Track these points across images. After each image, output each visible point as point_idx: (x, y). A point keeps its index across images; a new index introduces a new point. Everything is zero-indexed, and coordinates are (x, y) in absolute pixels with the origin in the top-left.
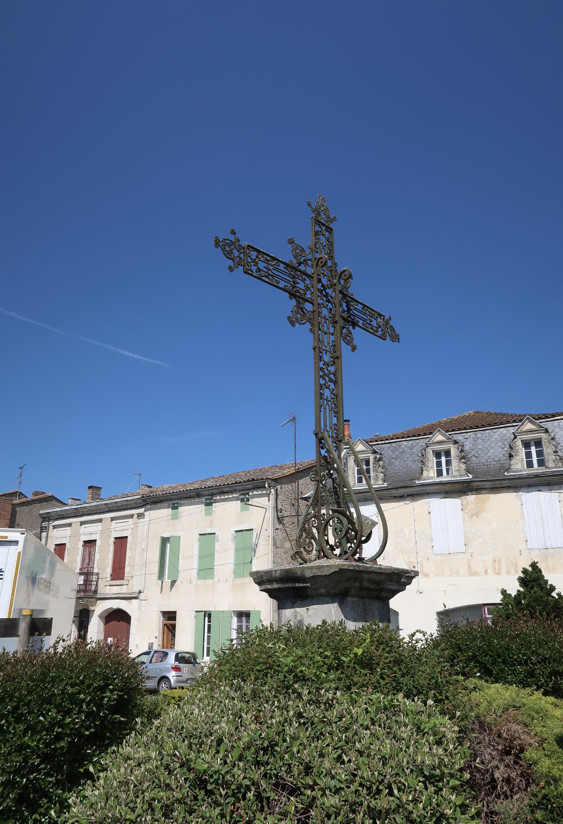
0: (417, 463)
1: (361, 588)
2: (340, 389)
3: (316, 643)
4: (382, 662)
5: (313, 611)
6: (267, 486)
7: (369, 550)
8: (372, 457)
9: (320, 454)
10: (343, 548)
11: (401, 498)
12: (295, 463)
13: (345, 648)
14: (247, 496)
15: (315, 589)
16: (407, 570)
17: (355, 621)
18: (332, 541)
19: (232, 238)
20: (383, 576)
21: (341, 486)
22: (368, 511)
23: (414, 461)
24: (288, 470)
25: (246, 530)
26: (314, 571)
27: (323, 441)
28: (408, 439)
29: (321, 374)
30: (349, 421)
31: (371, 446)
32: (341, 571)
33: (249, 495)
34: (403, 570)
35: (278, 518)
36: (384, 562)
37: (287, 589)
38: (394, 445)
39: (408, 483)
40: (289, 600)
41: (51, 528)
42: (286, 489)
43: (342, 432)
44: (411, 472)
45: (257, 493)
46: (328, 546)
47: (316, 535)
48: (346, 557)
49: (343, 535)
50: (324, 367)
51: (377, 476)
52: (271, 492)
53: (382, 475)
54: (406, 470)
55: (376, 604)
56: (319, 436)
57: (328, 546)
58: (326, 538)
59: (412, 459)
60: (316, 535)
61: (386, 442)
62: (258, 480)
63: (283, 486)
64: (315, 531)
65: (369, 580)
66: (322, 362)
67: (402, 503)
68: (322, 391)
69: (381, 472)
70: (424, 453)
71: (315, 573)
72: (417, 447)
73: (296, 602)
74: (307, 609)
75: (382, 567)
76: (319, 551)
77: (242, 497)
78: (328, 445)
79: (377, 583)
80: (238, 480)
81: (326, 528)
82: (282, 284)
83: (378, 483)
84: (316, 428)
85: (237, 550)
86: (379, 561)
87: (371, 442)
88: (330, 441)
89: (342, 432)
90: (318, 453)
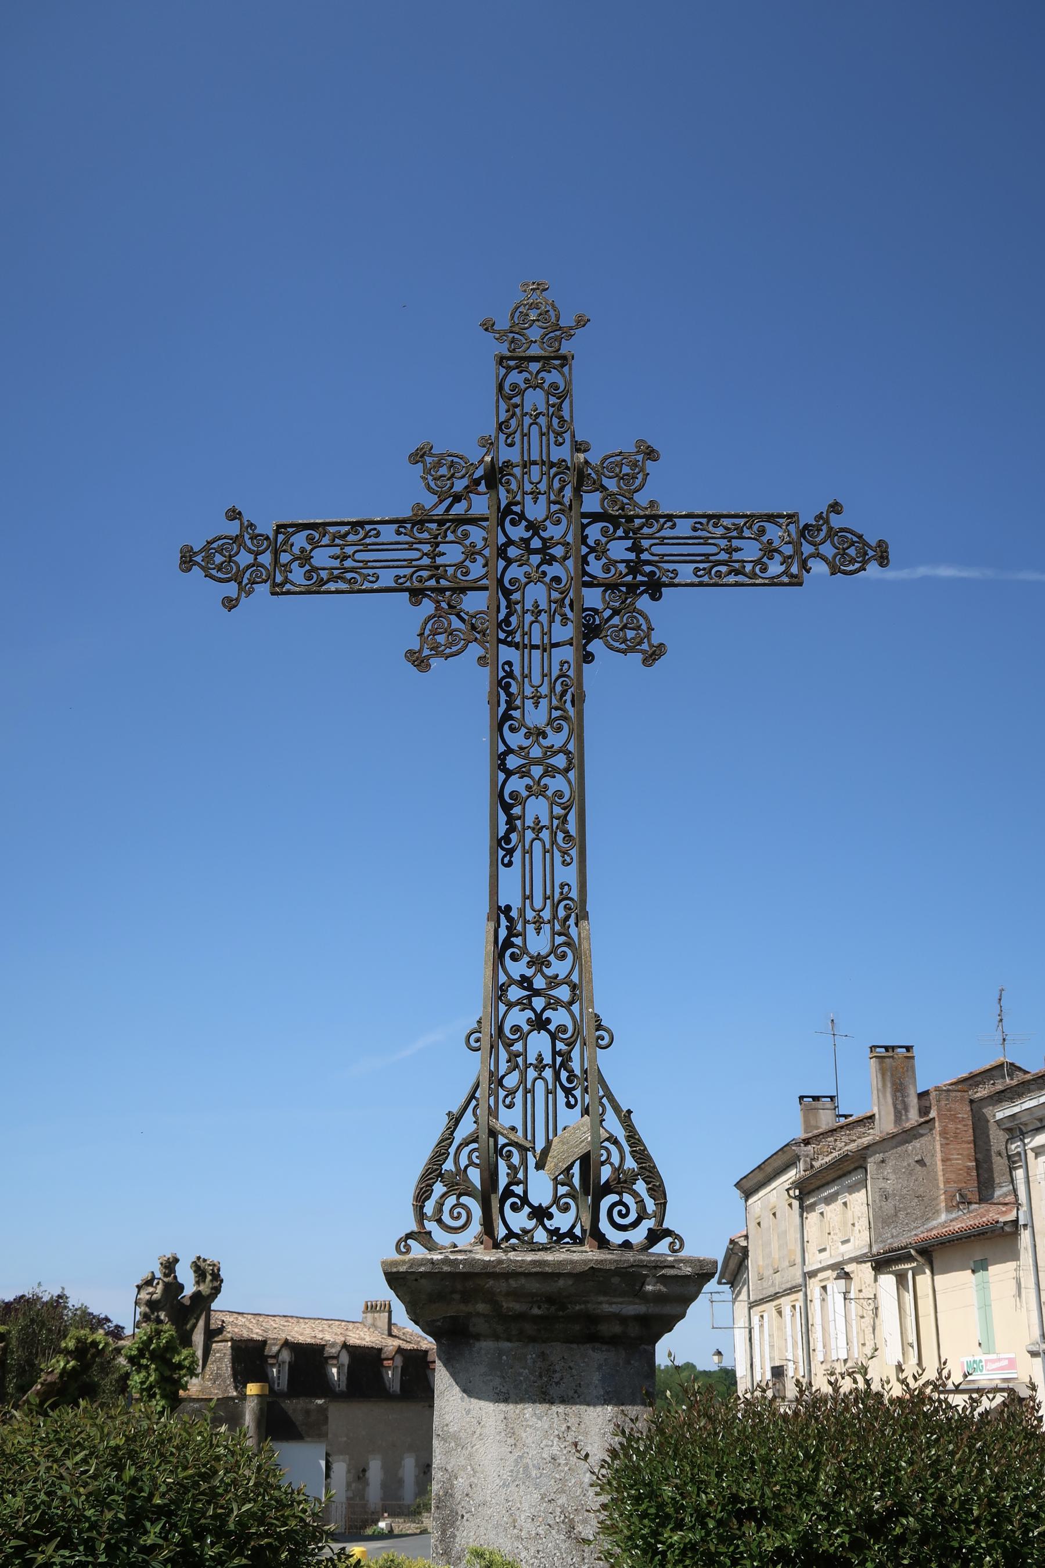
17: (506, 1401)
19: (233, 528)
20: (561, 1283)
41: (1031, 1155)
65: (515, 1295)
82: (387, 578)
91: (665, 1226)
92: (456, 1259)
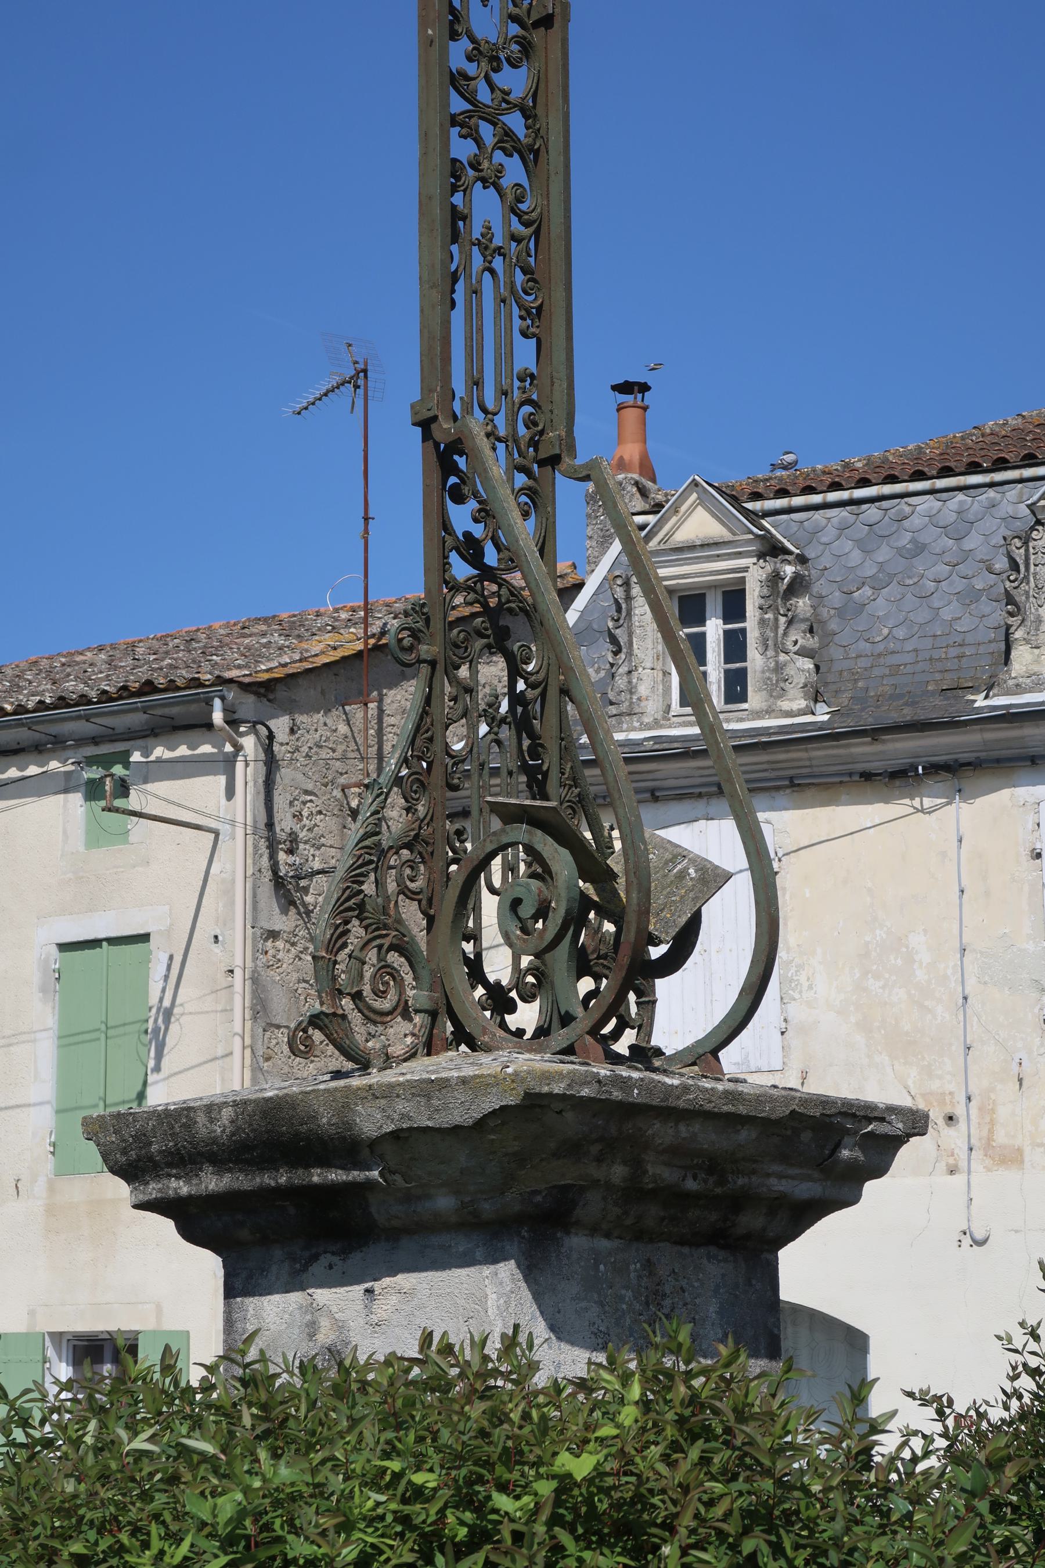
0: (985, 606)
1: (635, 1192)
2: (556, 187)
3: (369, 1431)
4: (689, 1514)
5: (394, 1299)
6: (218, 717)
7: (682, 1010)
8: (755, 577)
9: (446, 526)
10: (555, 1003)
11: (897, 779)
12: (367, 608)
13: (512, 1457)
14: (118, 770)
15: (408, 1198)
16: (870, 1107)
18: (499, 966)
20: (745, 1135)
21: (553, 693)
22: (710, 838)
23: (969, 597)
24: (329, 639)
25: (112, 941)
26: (401, 1106)
27: (461, 462)
28: (941, 483)
29: (458, 105)
30: (644, 388)
31: (754, 517)
32: (535, 1105)
33: (127, 765)
34: (847, 1103)
35: (278, 882)
36: (757, 1062)
37: (269, 1195)
38: (872, 512)
39: (933, 709)
40: (278, 1253)
42: (320, 734)
43: (560, 413)
44: (953, 652)
45: (168, 755)
46: (480, 991)
47: (421, 937)
48: (561, 1037)
49: (549, 936)
50: (471, 69)
51: (779, 668)
52: (238, 748)
53: (808, 664)
54: (928, 643)
55: (712, 1272)
56: (437, 435)
57: (480, 991)
58: (468, 947)
59: (960, 585)
60: (421, 937)
61: (833, 496)
62: (172, 686)
63: (301, 719)
64: (412, 915)
65: (675, 1152)
66: (464, 44)
67: (900, 807)
68: (458, 199)
69: (804, 653)
70: (1019, 555)
71: (403, 1116)
72: (989, 524)
73: (315, 1258)
74: (369, 1291)
75: (740, 1087)
76: (433, 1014)
77: (94, 773)
78: (486, 480)
79: (714, 1165)
80: (72, 687)
81: (467, 899)
83: (780, 705)
84: (426, 390)
85: (69, 1040)
86: (730, 1058)
87: (756, 496)
88: (496, 464)
89: (560, 413)
90: (436, 522)
91: (653, 1043)
92: (630, 1078)
